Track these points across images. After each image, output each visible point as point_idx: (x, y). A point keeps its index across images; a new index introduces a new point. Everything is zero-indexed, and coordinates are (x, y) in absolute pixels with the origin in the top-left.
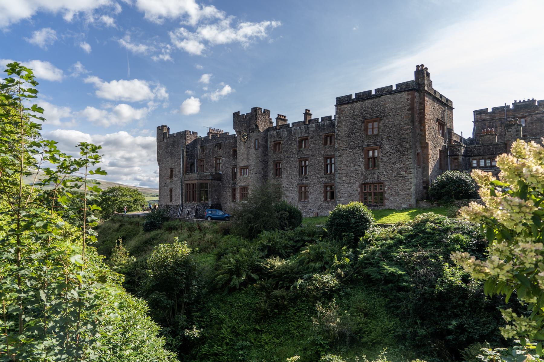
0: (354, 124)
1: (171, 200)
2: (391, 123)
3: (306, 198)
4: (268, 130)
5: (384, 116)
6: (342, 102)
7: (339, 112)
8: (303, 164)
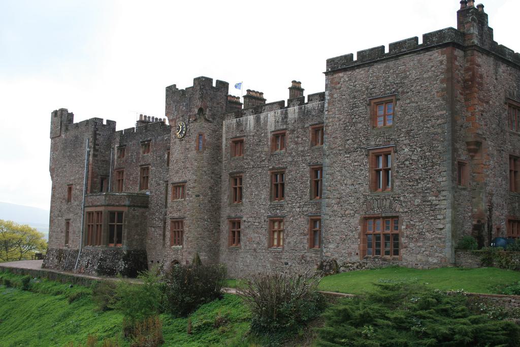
0: (355, 106)
1: (67, 242)
2: (414, 105)
5: (403, 93)
6: (338, 67)
8: (381, 166)
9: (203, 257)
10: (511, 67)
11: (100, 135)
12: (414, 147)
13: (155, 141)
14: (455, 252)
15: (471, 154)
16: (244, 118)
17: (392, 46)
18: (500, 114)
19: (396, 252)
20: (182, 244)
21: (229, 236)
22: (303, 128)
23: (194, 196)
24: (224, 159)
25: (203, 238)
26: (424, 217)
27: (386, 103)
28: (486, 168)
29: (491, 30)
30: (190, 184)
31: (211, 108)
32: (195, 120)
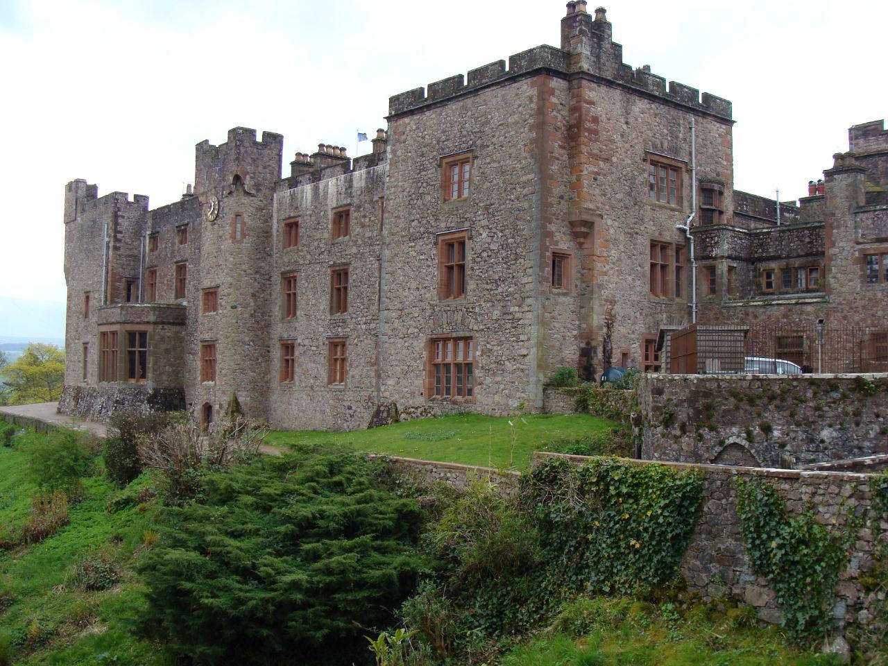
1: (85, 377)
5: (483, 147)
6: (406, 107)
10: (657, 104)
11: (123, 217)
12: (494, 230)
13: (193, 224)
14: (544, 390)
15: (578, 240)
16: (300, 187)
18: (634, 178)
21: (280, 367)
23: (229, 308)
24: (275, 251)
25: (243, 371)
26: (503, 339)
27: (462, 163)
28: (601, 262)
29: (617, 48)
30: (223, 291)
31: (254, 173)
32: (230, 193)
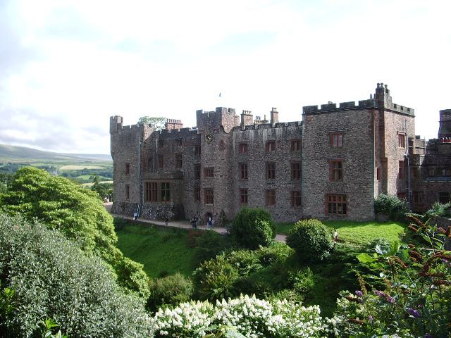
3: (274, 203)
4: (234, 129)
6: (309, 111)
7: (306, 121)
9: (226, 210)
17: (360, 102)
19: (345, 213)
20: (212, 203)
22: (286, 141)
